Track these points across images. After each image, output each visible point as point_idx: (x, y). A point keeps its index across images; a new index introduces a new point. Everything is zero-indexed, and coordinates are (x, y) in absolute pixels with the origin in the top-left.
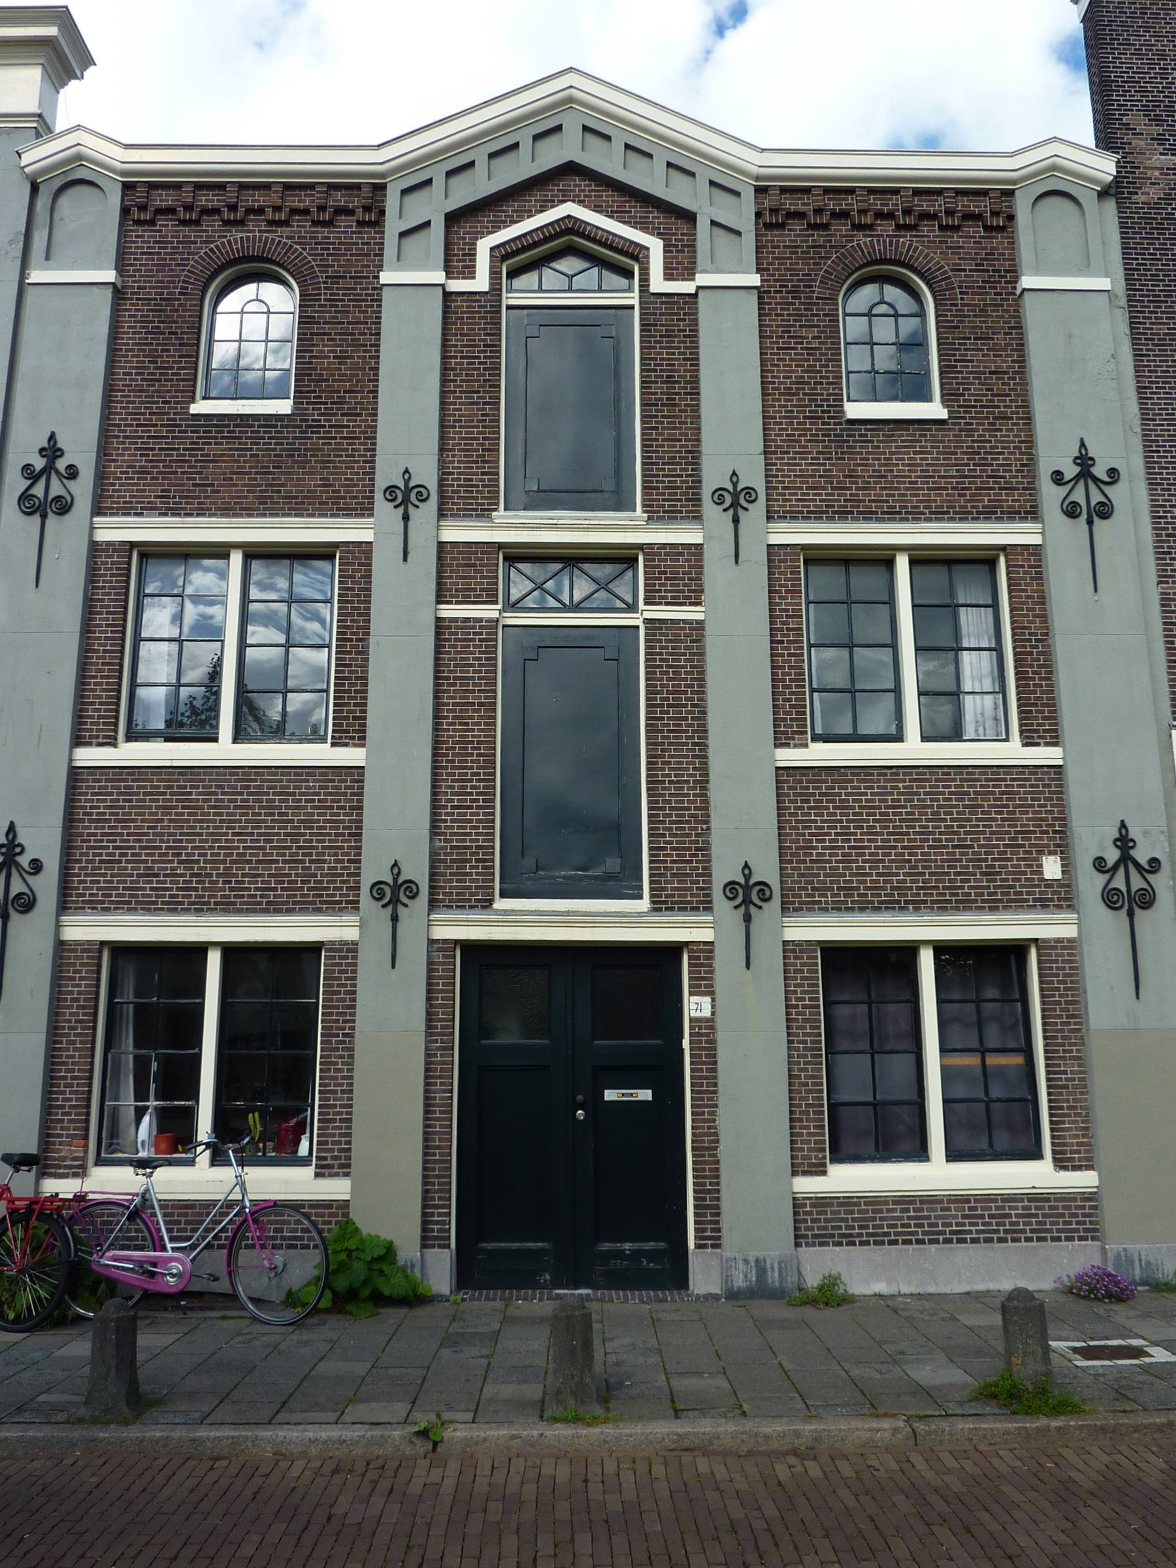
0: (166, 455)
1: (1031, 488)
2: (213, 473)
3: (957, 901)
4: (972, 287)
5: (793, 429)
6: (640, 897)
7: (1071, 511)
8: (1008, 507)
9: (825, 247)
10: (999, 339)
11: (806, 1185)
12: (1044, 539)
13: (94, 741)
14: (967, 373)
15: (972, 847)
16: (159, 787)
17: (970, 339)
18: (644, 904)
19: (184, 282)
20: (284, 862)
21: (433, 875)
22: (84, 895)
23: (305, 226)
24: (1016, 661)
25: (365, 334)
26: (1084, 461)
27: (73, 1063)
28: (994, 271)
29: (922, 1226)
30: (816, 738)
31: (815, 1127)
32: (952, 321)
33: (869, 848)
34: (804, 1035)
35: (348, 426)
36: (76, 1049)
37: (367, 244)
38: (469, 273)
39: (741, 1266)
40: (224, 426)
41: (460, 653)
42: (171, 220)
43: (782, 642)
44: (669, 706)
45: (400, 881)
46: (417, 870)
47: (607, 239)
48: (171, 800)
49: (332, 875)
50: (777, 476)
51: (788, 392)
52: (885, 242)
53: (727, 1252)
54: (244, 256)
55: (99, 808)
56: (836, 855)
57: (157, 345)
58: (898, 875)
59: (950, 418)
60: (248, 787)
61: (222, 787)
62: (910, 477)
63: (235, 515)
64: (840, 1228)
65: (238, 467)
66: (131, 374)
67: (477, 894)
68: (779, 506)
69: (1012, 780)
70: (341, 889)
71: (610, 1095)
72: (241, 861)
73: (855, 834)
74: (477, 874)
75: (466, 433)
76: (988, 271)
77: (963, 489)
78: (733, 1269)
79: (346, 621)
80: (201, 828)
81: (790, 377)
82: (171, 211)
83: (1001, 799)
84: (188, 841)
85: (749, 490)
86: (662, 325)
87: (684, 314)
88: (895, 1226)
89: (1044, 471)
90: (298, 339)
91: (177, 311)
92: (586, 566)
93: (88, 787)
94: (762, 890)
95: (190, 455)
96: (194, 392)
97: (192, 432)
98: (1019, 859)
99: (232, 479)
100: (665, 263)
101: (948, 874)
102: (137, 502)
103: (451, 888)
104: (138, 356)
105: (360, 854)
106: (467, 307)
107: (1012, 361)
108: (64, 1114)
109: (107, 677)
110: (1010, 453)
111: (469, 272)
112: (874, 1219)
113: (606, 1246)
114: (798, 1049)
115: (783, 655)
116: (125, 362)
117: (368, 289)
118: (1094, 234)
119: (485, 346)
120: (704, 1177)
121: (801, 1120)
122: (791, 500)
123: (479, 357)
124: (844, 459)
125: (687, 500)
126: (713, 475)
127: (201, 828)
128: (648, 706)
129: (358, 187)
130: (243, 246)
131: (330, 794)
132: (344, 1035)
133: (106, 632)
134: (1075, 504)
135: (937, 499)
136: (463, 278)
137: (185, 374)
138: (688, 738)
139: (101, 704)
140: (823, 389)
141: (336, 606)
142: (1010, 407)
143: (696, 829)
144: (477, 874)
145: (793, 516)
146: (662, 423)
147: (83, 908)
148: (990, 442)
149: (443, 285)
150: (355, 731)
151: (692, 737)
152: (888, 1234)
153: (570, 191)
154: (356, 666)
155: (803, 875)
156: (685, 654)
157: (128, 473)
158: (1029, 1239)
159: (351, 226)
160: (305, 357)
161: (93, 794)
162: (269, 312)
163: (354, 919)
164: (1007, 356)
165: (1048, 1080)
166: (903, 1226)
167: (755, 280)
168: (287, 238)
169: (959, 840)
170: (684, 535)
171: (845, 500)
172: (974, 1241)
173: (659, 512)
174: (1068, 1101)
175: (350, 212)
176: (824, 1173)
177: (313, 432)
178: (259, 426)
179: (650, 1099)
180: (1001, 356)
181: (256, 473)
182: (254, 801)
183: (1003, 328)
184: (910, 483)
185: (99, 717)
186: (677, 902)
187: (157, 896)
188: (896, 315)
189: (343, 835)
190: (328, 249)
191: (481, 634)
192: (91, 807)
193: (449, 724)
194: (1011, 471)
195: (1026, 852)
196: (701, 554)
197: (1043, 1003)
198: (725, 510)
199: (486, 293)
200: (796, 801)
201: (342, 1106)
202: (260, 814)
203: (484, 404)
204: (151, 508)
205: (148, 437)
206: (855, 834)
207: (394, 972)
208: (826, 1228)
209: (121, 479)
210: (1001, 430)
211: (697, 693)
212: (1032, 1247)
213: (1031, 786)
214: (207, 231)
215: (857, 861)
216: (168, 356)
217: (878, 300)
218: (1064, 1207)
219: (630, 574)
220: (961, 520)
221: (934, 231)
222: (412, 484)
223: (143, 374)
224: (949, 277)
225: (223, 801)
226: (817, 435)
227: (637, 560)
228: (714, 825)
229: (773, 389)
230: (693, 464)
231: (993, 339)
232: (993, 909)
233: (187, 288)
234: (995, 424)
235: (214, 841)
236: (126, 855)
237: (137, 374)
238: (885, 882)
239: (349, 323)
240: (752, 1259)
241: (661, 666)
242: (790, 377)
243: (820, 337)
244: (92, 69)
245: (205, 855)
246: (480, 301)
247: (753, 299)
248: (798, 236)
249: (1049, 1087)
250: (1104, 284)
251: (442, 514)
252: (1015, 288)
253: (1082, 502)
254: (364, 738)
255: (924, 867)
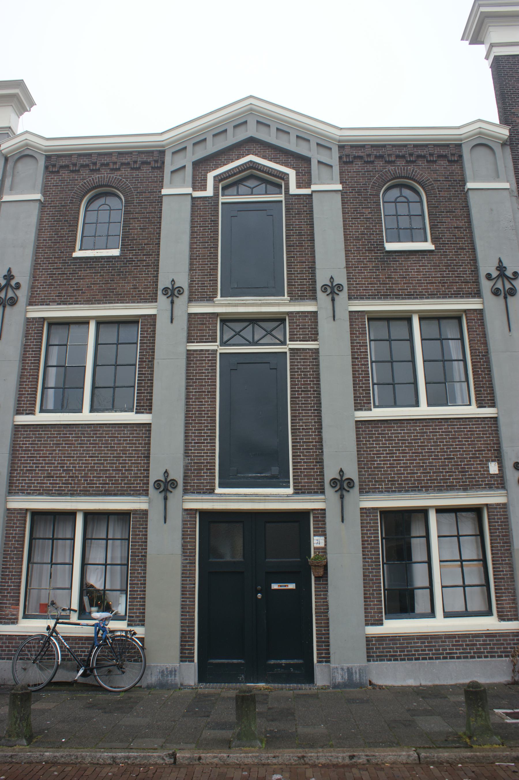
0: (61, 277)
1: (477, 282)
2: (83, 284)
3: (447, 486)
4: (444, 188)
5: (360, 256)
6: (289, 487)
7: (496, 292)
8: (466, 291)
9: (373, 171)
10: (458, 212)
11: (373, 630)
12: (484, 306)
13: (24, 412)
14: (443, 228)
15: (453, 458)
16: (54, 434)
17: (444, 212)
18: (290, 491)
19: (72, 198)
20: (113, 470)
21: (185, 477)
22: (18, 486)
23: (128, 170)
24: (473, 366)
25: (155, 218)
26: (501, 268)
27: (13, 568)
28: (454, 181)
29: (431, 650)
30: (375, 407)
31: (377, 601)
32: (435, 204)
33: (403, 460)
34: (371, 555)
35: (146, 260)
36: (14, 561)
37: (156, 177)
38: (204, 188)
39: (340, 671)
40: (88, 262)
41: (199, 367)
42: (67, 170)
43: (358, 358)
44: (302, 391)
45: (168, 480)
46: (177, 474)
47: (269, 171)
48: (60, 440)
49: (136, 477)
50: (353, 278)
51: (357, 239)
52: (401, 169)
53: (332, 665)
54: (99, 185)
55: (26, 444)
56: (387, 464)
57: (59, 226)
58: (417, 473)
59: (436, 249)
60: (96, 434)
61: (84, 434)
62: (418, 278)
63: (92, 304)
64: (390, 652)
65: (94, 281)
66: (46, 240)
67: (207, 486)
68: (354, 293)
69: (473, 425)
70: (140, 484)
71: (275, 586)
72: (92, 470)
73: (396, 453)
74: (207, 476)
75: (202, 262)
76: (451, 181)
77: (444, 283)
78: (336, 673)
79: (143, 352)
80: (74, 454)
81: (358, 232)
82: (67, 166)
83: (467, 434)
84: (67, 460)
85: (339, 286)
86: (295, 209)
87: (306, 204)
88: (418, 651)
89: (483, 273)
90: (124, 221)
91: (68, 211)
92: (261, 324)
93: (21, 434)
94: (349, 482)
95: (72, 276)
96: (75, 247)
97: (73, 265)
98: (477, 464)
99: (91, 287)
100: (296, 180)
101: (442, 472)
102: (47, 299)
103: (194, 483)
104: (50, 232)
105: (149, 467)
106: (203, 204)
107: (465, 222)
108: (8, 593)
109: (31, 381)
110: (465, 266)
111: (204, 188)
112: (407, 647)
113: (272, 662)
114: (368, 562)
115: (358, 365)
116: (44, 235)
117: (156, 197)
118: (500, 163)
119: (211, 221)
120: (321, 627)
121: (370, 598)
122: (360, 290)
123: (208, 226)
124: (385, 270)
125: (309, 290)
126: (321, 279)
127: (74, 454)
128: (291, 391)
129: (152, 152)
130: (99, 181)
131: (135, 437)
132: (142, 556)
133: (31, 360)
134: (498, 289)
135: (432, 288)
136: (201, 191)
137: (71, 239)
138: (311, 407)
139: (28, 394)
140: (374, 237)
141: (139, 345)
142: (465, 244)
143: (316, 452)
144: (207, 476)
145: (361, 297)
146: (297, 254)
147: (18, 493)
148: (456, 260)
149: (191, 194)
150: (147, 406)
151: (314, 407)
152: (414, 655)
153: (251, 150)
154: (148, 374)
155: (370, 475)
156: (309, 365)
157: (43, 285)
158: (486, 657)
159: (149, 170)
160: (126, 229)
161: (24, 438)
162: (110, 210)
163: (143, 498)
164: (462, 220)
165: (494, 575)
166: (422, 650)
167: (339, 187)
168: (120, 176)
169: (447, 455)
170: (308, 307)
171: (387, 289)
172: (458, 658)
173: (296, 296)
174: (504, 586)
175: (148, 163)
176: (382, 624)
177: (129, 264)
178: (104, 262)
179: (295, 588)
180: (459, 220)
181: (102, 284)
182: (99, 440)
183: (459, 207)
184: (418, 280)
185: (27, 401)
186: (307, 489)
187: (53, 487)
188: (408, 202)
189: (141, 457)
190: (138, 180)
191: (209, 357)
192: (23, 444)
193: (193, 402)
194: (466, 274)
195: (480, 461)
196: (317, 316)
197: (491, 536)
198: (328, 295)
199: (211, 197)
200: (366, 438)
201: (141, 591)
202: (101, 447)
203: (211, 248)
204: (54, 302)
205: (53, 269)
206: (396, 453)
207: (165, 525)
208: (383, 652)
209: (40, 288)
210: (461, 255)
211: (315, 384)
212: (488, 661)
213: (482, 427)
214: (83, 175)
215: (397, 467)
216: (63, 231)
217: (399, 195)
218: (504, 640)
219: (282, 326)
220: (443, 298)
221: (424, 163)
222: (175, 286)
223: (52, 240)
224: (432, 184)
225: (84, 440)
226: (372, 259)
227: (285, 320)
228: (325, 450)
229: (350, 237)
230: (311, 273)
231: (455, 212)
232: (465, 490)
233: (73, 200)
234: (458, 252)
235: (80, 460)
236: (38, 467)
237: (49, 240)
238: (411, 477)
239: (147, 213)
240: (345, 668)
241: (298, 372)
242: (358, 232)
243: (372, 213)
244: (34, 107)
245: (75, 467)
246: (209, 201)
247: (339, 197)
248: (359, 167)
249: (495, 579)
250: (507, 185)
251: (190, 300)
252: (464, 188)
253: (501, 288)
254: (151, 409)
255: (430, 469)
